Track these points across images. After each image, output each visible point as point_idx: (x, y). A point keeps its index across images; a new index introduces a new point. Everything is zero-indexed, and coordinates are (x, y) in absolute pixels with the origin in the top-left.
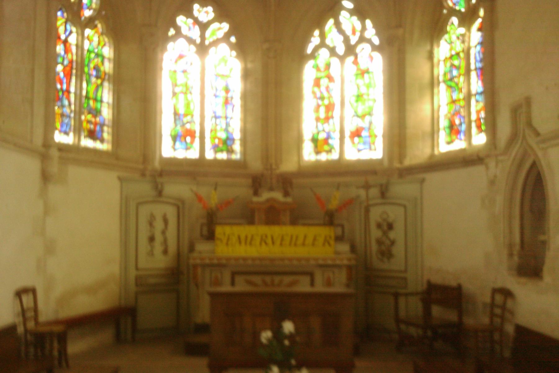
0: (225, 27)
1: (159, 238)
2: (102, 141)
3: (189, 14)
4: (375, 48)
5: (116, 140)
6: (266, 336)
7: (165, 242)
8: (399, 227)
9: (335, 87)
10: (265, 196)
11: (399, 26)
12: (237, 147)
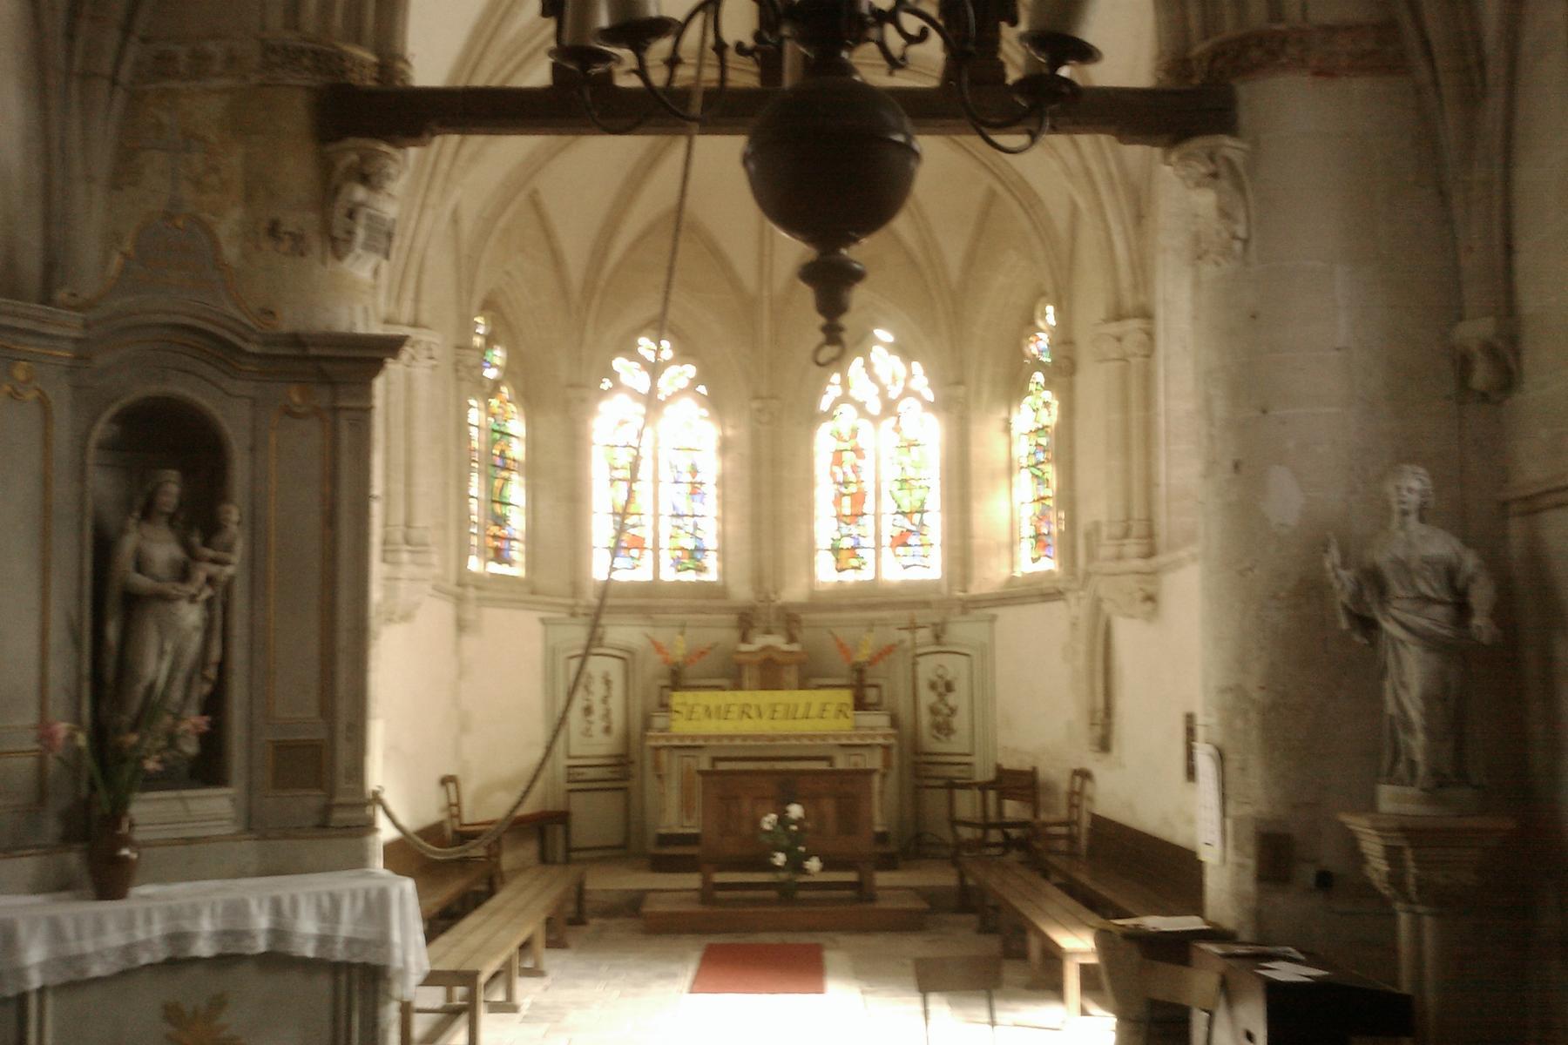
0: (690, 370)
1: (598, 709)
2: (510, 562)
3: (630, 351)
4: (928, 406)
5: (531, 564)
6: (769, 821)
7: (607, 715)
8: (961, 686)
9: (867, 466)
10: (759, 641)
11: (959, 382)
12: (711, 562)
